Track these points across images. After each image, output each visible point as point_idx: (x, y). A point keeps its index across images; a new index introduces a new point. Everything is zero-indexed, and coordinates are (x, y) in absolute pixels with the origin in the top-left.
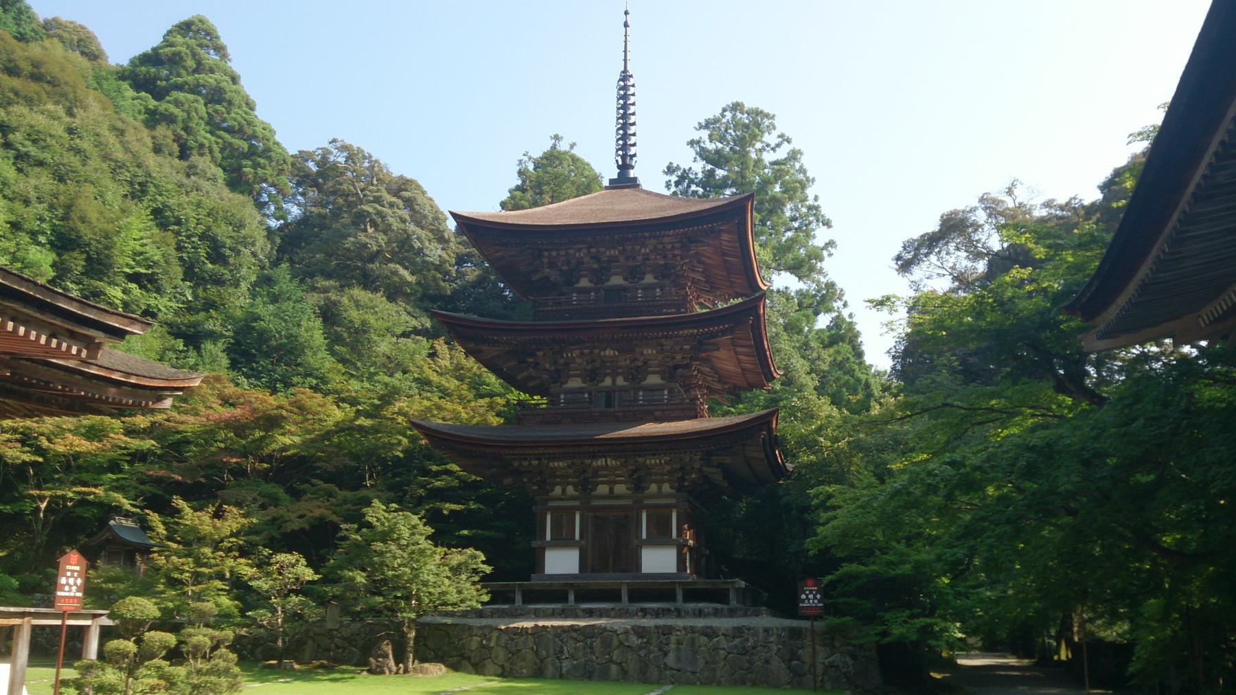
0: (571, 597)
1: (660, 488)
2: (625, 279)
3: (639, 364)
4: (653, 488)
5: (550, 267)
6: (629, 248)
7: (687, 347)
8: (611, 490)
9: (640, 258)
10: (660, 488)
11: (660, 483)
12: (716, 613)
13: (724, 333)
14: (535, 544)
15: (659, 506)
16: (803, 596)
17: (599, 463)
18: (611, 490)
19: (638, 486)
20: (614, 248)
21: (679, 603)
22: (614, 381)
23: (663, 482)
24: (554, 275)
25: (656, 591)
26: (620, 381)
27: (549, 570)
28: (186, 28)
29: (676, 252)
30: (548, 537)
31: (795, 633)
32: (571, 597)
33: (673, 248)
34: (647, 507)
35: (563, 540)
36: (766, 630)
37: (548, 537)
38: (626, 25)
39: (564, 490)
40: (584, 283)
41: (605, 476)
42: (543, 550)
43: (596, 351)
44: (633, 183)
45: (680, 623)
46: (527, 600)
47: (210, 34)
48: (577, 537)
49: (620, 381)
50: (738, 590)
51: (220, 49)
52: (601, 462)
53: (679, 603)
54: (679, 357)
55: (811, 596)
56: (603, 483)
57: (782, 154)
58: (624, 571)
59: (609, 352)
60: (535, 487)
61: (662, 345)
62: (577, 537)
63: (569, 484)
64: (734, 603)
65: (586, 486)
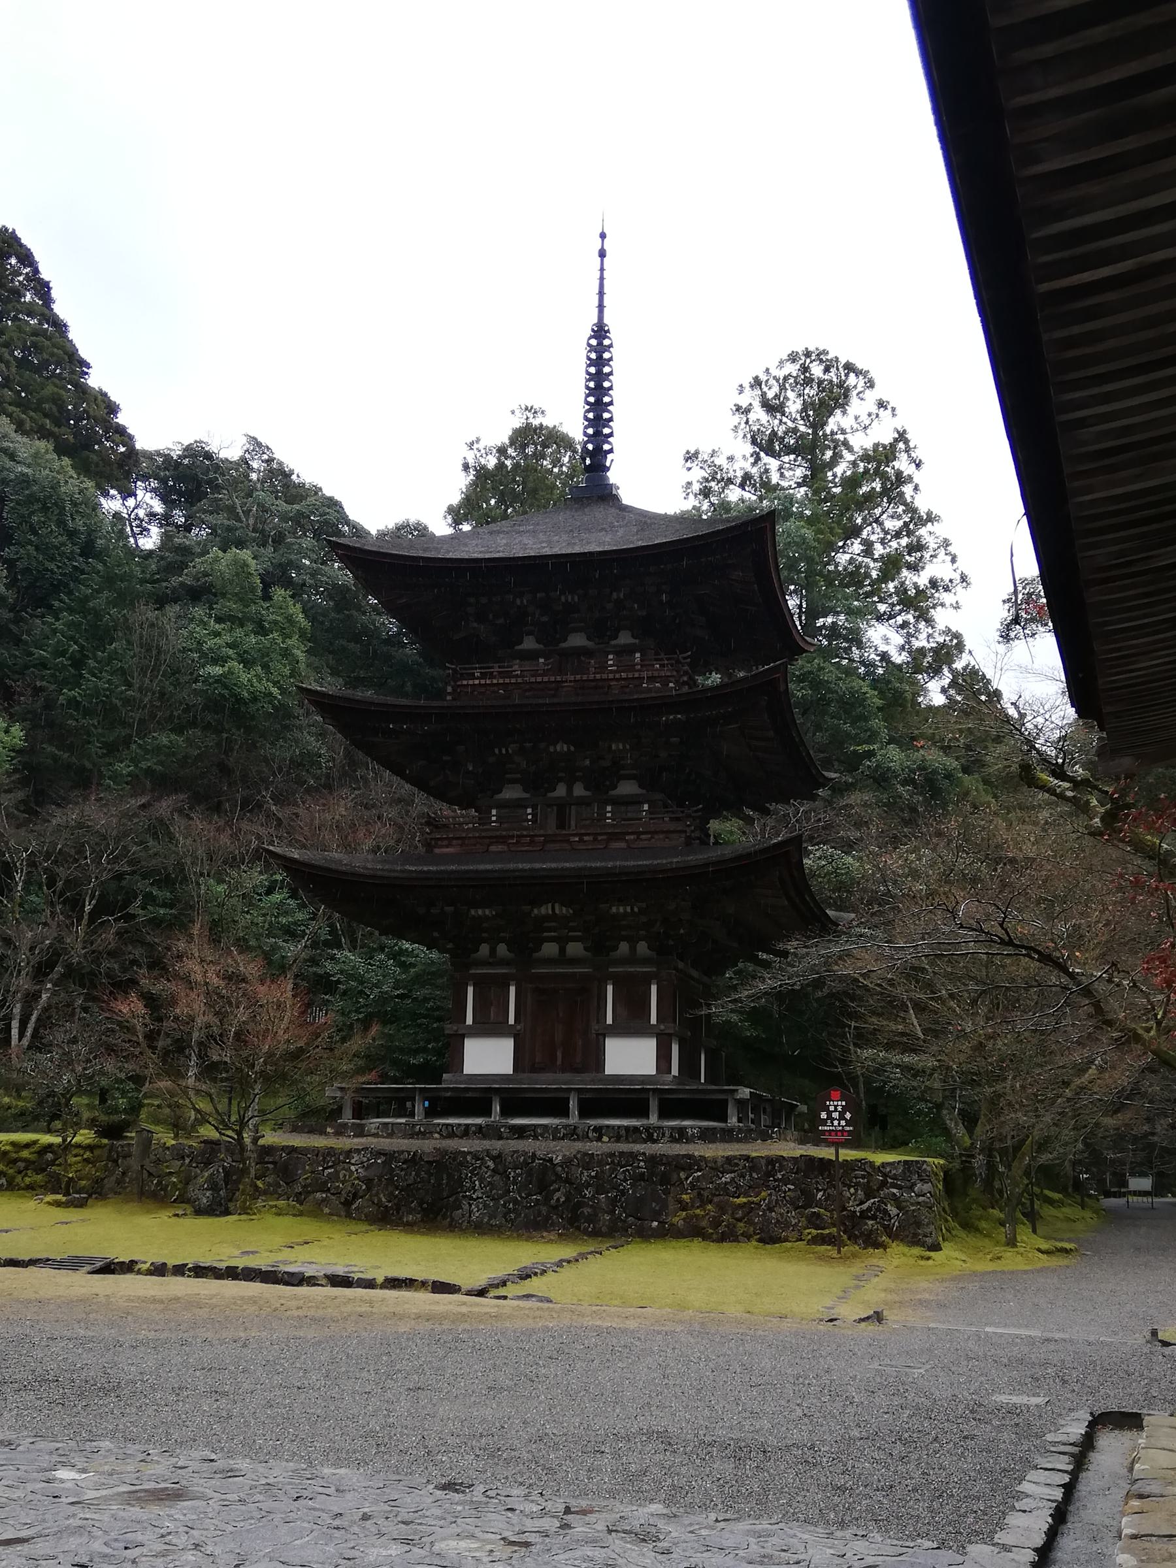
0: (497, 1108)
1: (633, 949)
2: (589, 639)
4: (624, 947)
8: (562, 950)
10: (633, 949)
12: (706, 1136)
16: (824, 1115)
17: (543, 911)
18: (562, 950)
22: (570, 790)
25: (627, 1098)
30: (469, 1020)
32: (497, 1108)
35: (489, 1027)
37: (469, 1020)
38: (602, 254)
39: (493, 951)
40: (529, 643)
41: (549, 930)
42: (463, 1037)
43: (542, 745)
44: (605, 495)
46: (587, 1110)
48: (511, 1021)
49: (579, 790)
50: (741, 1103)
52: (546, 910)
55: (835, 1115)
57: (882, 433)
62: (511, 1021)
63: (502, 940)
64: (733, 1121)
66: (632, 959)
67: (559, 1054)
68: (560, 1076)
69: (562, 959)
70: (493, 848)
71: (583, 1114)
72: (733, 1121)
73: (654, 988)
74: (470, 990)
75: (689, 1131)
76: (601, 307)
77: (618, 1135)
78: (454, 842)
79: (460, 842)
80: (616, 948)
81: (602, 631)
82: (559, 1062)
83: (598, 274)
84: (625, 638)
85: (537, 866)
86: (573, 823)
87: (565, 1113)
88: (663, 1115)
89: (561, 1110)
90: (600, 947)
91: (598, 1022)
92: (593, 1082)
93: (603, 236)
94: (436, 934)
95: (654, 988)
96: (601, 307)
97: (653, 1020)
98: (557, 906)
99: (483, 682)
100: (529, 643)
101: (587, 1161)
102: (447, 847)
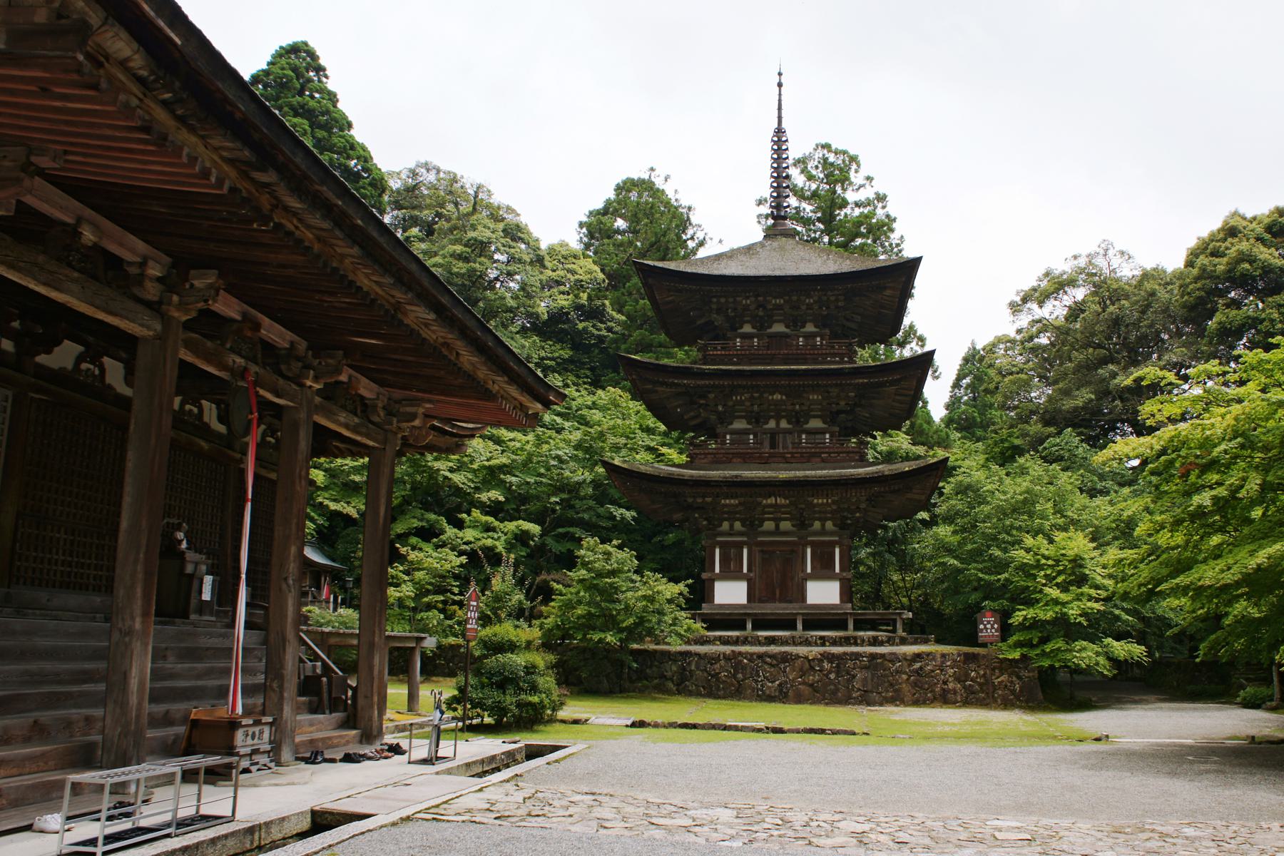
0: (749, 626)
1: (823, 525)
3: (805, 408)
4: (817, 525)
6: (795, 298)
8: (777, 526)
9: (804, 307)
10: (823, 525)
13: (892, 383)
14: (704, 576)
16: (982, 626)
17: (769, 501)
18: (777, 526)
22: (778, 424)
24: (718, 320)
25: (821, 619)
27: (719, 599)
28: (295, 49)
30: (717, 570)
31: (970, 658)
32: (749, 626)
33: (837, 300)
35: (731, 573)
36: (943, 656)
37: (717, 570)
38: (780, 85)
39: (732, 526)
40: (747, 329)
42: (712, 581)
45: (802, 650)
47: (312, 55)
48: (745, 570)
49: (784, 424)
51: (320, 69)
52: (771, 501)
54: (842, 403)
56: (769, 519)
58: (791, 602)
59: (777, 397)
62: (745, 570)
64: (900, 632)
65: (752, 525)
66: (823, 532)
68: (777, 604)
69: (778, 532)
71: (856, 629)
72: (900, 632)
73: (837, 551)
74: (717, 551)
76: (780, 118)
81: (796, 322)
84: (810, 328)
85: (808, 473)
87: (794, 628)
89: (790, 625)
90: (802, 524)
93: (780, 74)
95: (837, 551)
96: (780, 118)
97: (837, 570)
100: (747, 329)
101: (831, 657)
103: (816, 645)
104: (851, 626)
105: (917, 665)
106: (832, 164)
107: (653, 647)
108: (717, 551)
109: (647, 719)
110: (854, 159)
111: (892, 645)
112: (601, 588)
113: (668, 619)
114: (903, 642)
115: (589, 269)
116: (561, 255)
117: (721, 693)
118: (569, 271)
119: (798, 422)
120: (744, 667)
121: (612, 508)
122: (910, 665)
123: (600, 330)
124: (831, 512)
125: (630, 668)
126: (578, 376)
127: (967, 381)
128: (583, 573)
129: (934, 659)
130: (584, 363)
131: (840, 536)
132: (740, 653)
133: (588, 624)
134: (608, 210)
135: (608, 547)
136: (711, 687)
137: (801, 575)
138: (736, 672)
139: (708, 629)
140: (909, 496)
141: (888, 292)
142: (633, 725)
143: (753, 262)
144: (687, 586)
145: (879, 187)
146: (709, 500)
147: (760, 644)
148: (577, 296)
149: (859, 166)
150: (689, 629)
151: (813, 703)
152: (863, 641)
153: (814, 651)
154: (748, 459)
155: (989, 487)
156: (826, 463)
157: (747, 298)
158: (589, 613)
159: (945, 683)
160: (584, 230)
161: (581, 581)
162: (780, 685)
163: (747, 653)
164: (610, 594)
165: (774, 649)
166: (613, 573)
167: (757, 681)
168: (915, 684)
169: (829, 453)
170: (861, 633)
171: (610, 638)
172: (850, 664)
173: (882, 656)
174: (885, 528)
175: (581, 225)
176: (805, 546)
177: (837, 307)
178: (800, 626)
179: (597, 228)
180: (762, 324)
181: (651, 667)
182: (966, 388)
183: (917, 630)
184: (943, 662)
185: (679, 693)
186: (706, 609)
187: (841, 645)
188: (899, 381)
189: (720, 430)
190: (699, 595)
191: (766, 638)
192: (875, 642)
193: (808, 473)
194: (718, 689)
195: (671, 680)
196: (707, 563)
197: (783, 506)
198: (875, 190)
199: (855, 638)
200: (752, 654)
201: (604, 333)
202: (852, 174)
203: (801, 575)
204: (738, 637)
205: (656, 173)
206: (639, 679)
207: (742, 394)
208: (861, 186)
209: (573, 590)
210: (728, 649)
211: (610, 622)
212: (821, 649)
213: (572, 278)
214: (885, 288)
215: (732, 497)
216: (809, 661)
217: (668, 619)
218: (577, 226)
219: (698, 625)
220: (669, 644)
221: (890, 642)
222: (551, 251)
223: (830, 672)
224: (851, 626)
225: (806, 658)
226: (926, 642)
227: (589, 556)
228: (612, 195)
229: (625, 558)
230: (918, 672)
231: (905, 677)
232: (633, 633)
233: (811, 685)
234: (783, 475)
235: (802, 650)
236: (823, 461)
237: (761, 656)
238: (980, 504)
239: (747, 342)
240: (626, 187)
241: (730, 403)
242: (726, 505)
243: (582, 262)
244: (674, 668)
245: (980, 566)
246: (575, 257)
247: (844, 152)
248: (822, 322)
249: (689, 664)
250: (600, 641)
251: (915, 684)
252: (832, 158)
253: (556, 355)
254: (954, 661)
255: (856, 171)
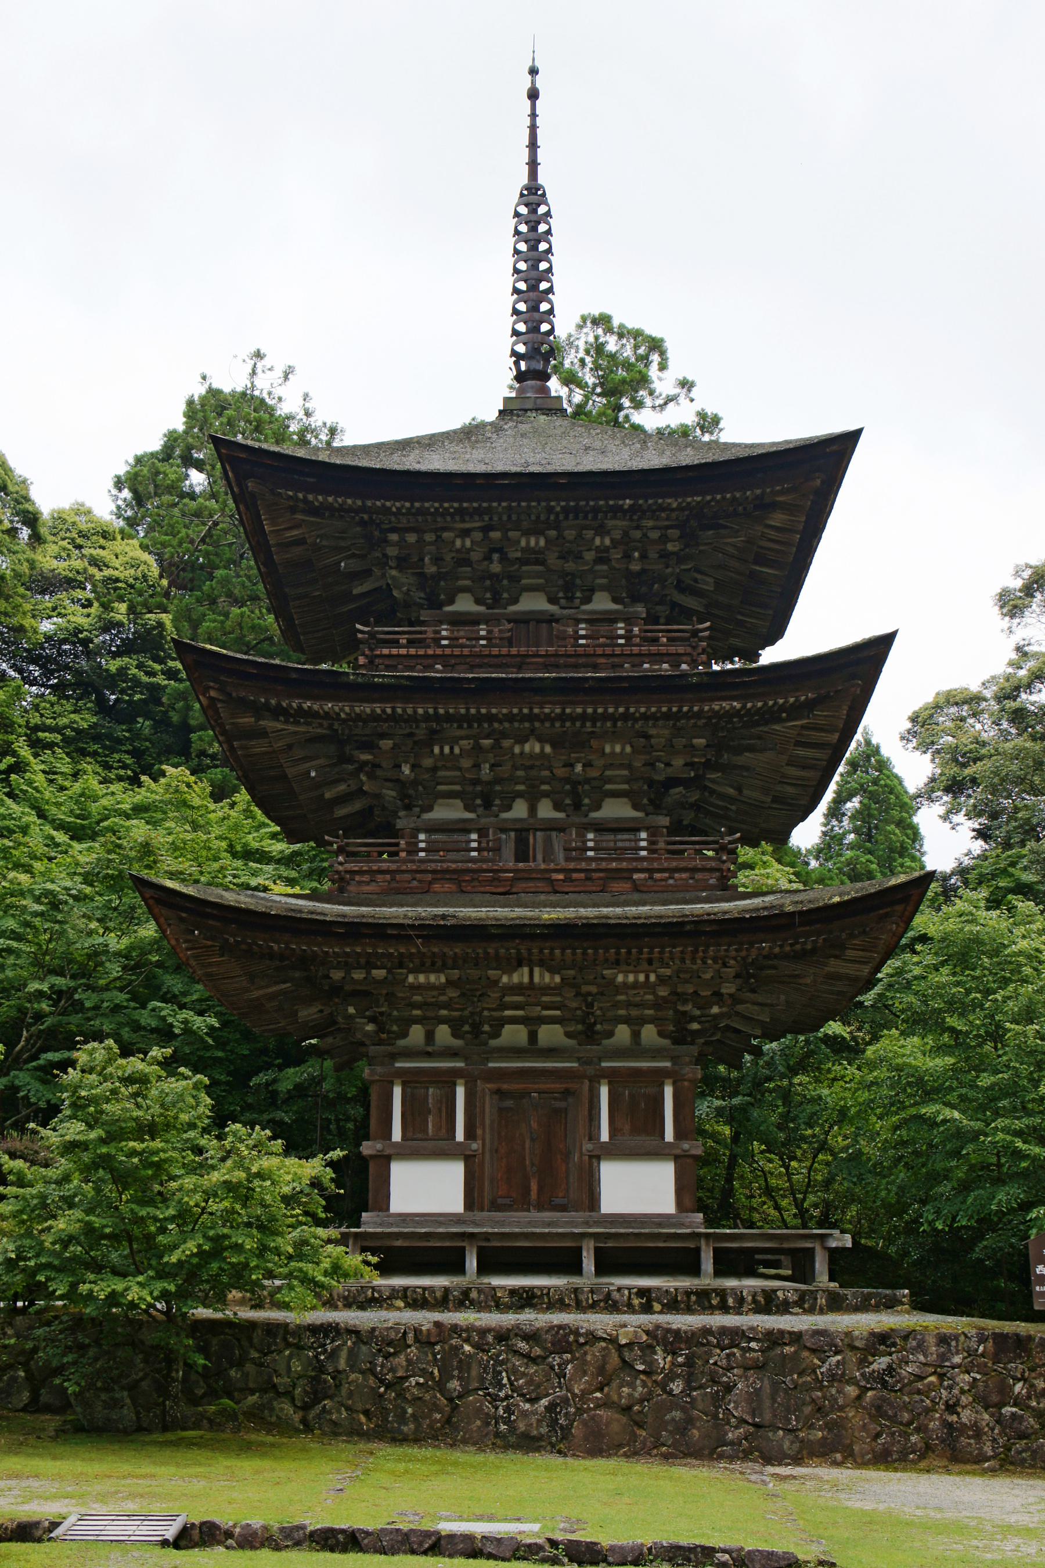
0: (472, 1263)
1: (636, 1035)
4: (623, 1033)
5: (399, 568)
7: (700, 742)
8: (533, 1036)
9: (589, 556)
10: (636, 1035)
11: (430, 1023)
13: (796, 711)
14: (367, 1148)
15: (637, 1073)
17: (516, 978)
18: (533, 1036)
19: (589, 1033)
20: (538, 533)
21: (588, 1277)
22: (533, 810)
23: (643, 1021)
24: (403, 584)
25: (634, 1250)
26: (546, 811)
29: (670, 547)
30: (397, 1135)
32: (472, 1263)
34: (401, 1073)
35: (427, 1143)
36: (943, 1340)
37: (397, 1135)
38: (533, 95)
39: (430, 1036)
42: (385, 1160)
45: (600, 1322)
48: (460, 1136)
49: (546, 811)
50: (835, 1255)
52: (521, 976)
53: (588, 1277)
54: (678, 762)
56: (514, 1021)
58: (563, 1208)
59: (533, 747)
60: (370, 1027)
61: (647, 737)
62: (460, 1136)
65: (476, 1031)
66: (635, 1049)
67: (534, 1187)
68: (535, 1215)
69: (533, 1048)
70: (437, 887)
73: (668, 1092)
74: (397, 1092)
75: (780, 1294)
76: (533, 165)
77: (418, 1301)
78: (380, 877)
79: (388, 877)
80: (611, 1034)
81: (570, 589)
82: (534, 1195)
83: (528, 122)
84: (602, 603)
85: (605, 911)
86: (540, 857)
87: (576, 1269)
88: (718, 1273)
89: (455, 1265)
91: (590, 1139)
92: (587, 1224)
93: (533, 71)
94: (351, 1010)
95: (668, 1092)
96: (533, 165)
97: (669, 1135)
98: (537, 970)
99: (412, 651)
100: (464, 604)
101: (672, 1340)
102: (368, 883)
103: (631, 1309)
104: (708, 1264)
105: (881, 1363)
106: (612, 356)
107: (247, 1314)
108: (397, 1092)
109: (225, 1519)
110: (656, 345)
111: (811, 1311)
112: (124, 1172)
113: (286, 1243)
114: (836, 1304)
115: (133, 558)
116: (80, 532)
117: (408, 1428)
118: (94, 562)
119: (577, 806)
120: (465, 1364)
121: (167, 1010)
122: (863, 1362)
123: (151, 674)
124: (657, 1005)
125: (189, 1366)
126: (107, 767)
127: (853, 805)
128: (74, 1130)
129: (921, 1347)
130: (119, 741)
131: (674, 1059)
132: (455, 1329)
133: (87, 1255)
134: (176, 450)
135: (135, 1064)
136: (385, 1412)
137: (588, 1146)
138: (446, 1375)
139: (384, 1269)
140: (834, 966)
141: (778, 519)
142: (188, 1538)
143: (478, 454)
144: (330, 1164)
145: (706, 400)
146: (379, 973)
147: (499, 1306)
148: (106, 607)
149: (662, 353)
150: (336, 1270)
151: (633, 1454)
152: (741, 1300)
153: (632, 1324)
154: (465, 882)
155: (1023, 944)
156: (641, 892)
157: (465, 533)
158: (89, 1230)
159: (951, 1408)
160: (126, 494)
161: (71, 1147)
162: (551, 1408)
163: (470, 1329)
164: (144, 1181)
165: (529, 1318)
166: (151, 1130)
167: (495, 1398)
168: (878, 1411)
169: (650, 871)
170: (731, 1283)
171: (136, 1291)
172: (718, 1357)
173: (796, 1337)
174: (757, 1052)
175: (119, 484)
176: (594, 1082)
177: (664, 555)
178: (589, 1264)
179: (147, 484)
180: (496, 592)
181: (240, 1364)
182: (853, 818)
183: (864, 1273)
184: (943, 1357)
185: (307, 1427)
186: (370, 1222)
187: (689, 1310)
188: (811, 705)
189: (403, 822)
190: (356, 1191)
191: (513, 1292)
192: (768, 1304)
193: (605, 911)
194: (402, 1418)
195: (289, 1394)
196: (369, 1122)
197: (546, 989)
198: (697, 406)
199: (722, 1293)
200: (483, 1332)
201: (161, 680)
202: (653, 372)
203: (588, 1146)
204: (447, 1290)
205: (267, 362)
206: (213, 1394)
207: (453, 741)
208: (670, 399)
209: (51, 1173)
210: (425, 1319)
211: (143, 1251)
212: (644, 1319)
213: (99, 576)
214: (773, 506)
215: (433, 968)
216: (620, 1348)
217: (286, 1243)
218: (110, 484)
219: (354, 1260)
220: (285, 1306)
221: (805, 1303)
222: (59, 518)
223: (671, 1377)
224: (708, 1264)
225: (613, 1340)
226: (890, 1304)
227: (92, 1086)
228: (179, 424)
229: (186, 1093)
230: (881, 1379)
231: (852, 1391)
232: (191, 1279)
233: (627, 1409)
234: (549, 915)
235: (600, 1322)
236: (636, 888)
237: (503, 1336)
238: (1005, 982)
239: (462, 632)
240: (210, 410)
241: (428, 762)
242: (417, 988)
243: (119, 545)
244: (297, 1366)
245: (1018, 1125)
246: (105, 535)
247: (637, 334)
248: (631, 589)
249: (333, 1355)
250: (113, 1298)
251: (878, 1411)
252: (612, 344)
253: (63, 721)
254: (971, 1353)
255: (663, 367)
